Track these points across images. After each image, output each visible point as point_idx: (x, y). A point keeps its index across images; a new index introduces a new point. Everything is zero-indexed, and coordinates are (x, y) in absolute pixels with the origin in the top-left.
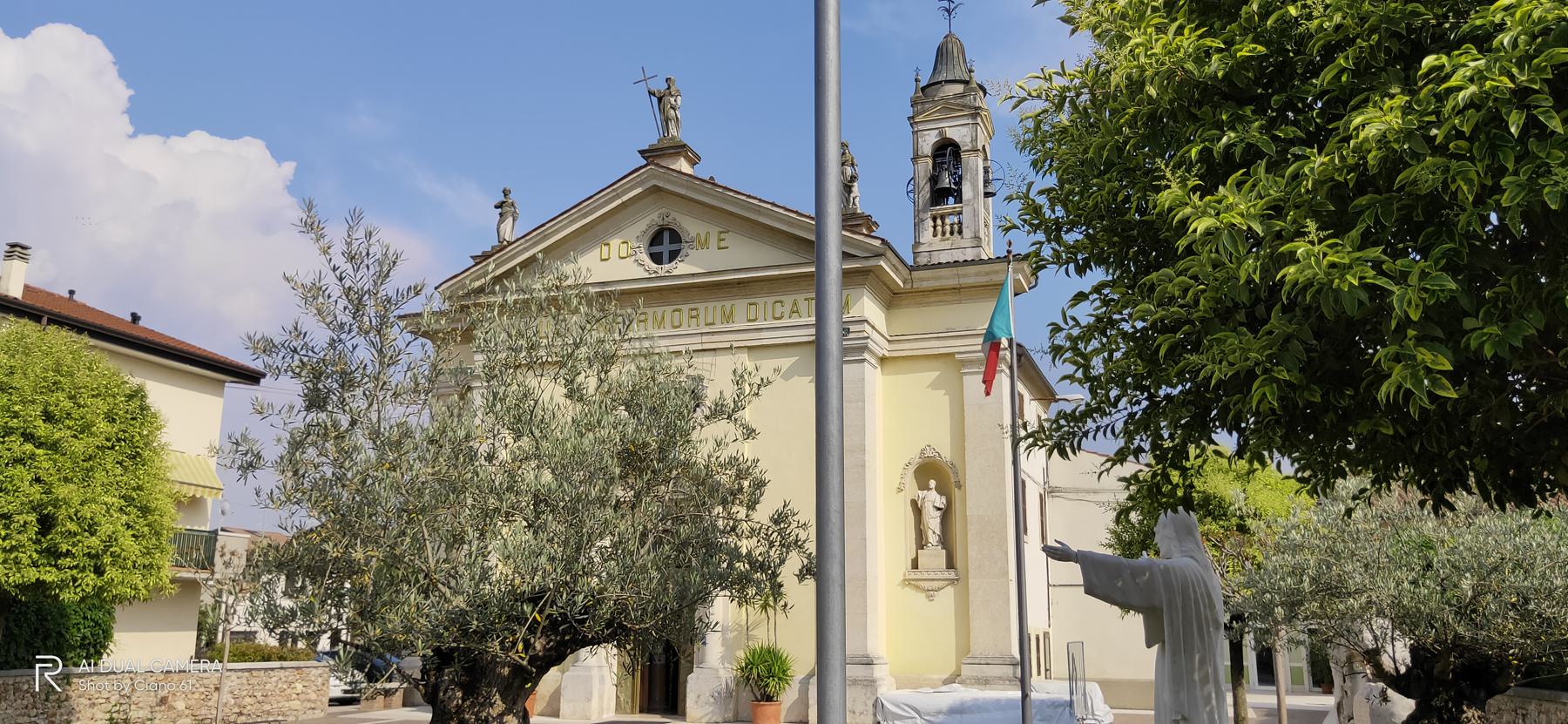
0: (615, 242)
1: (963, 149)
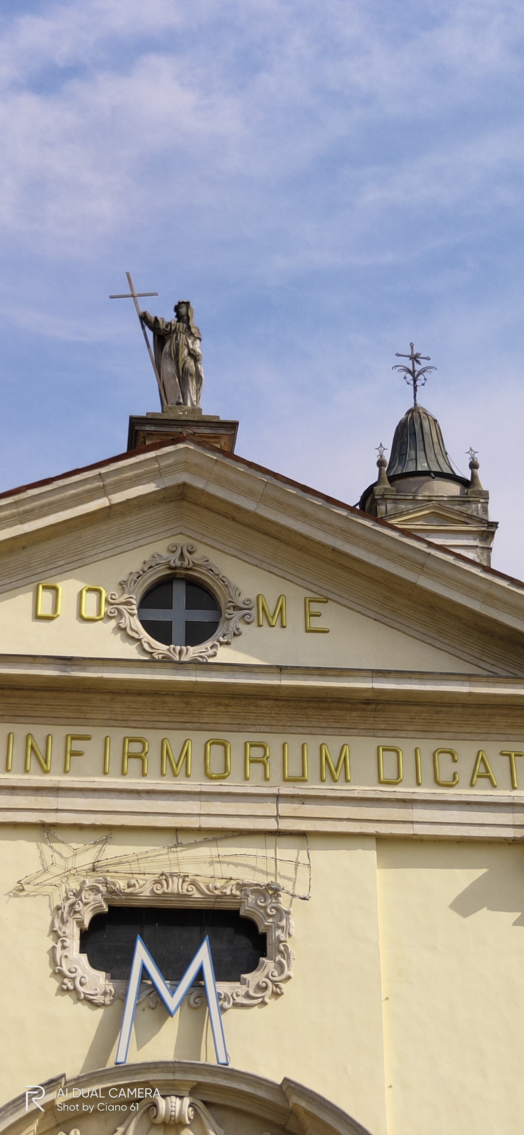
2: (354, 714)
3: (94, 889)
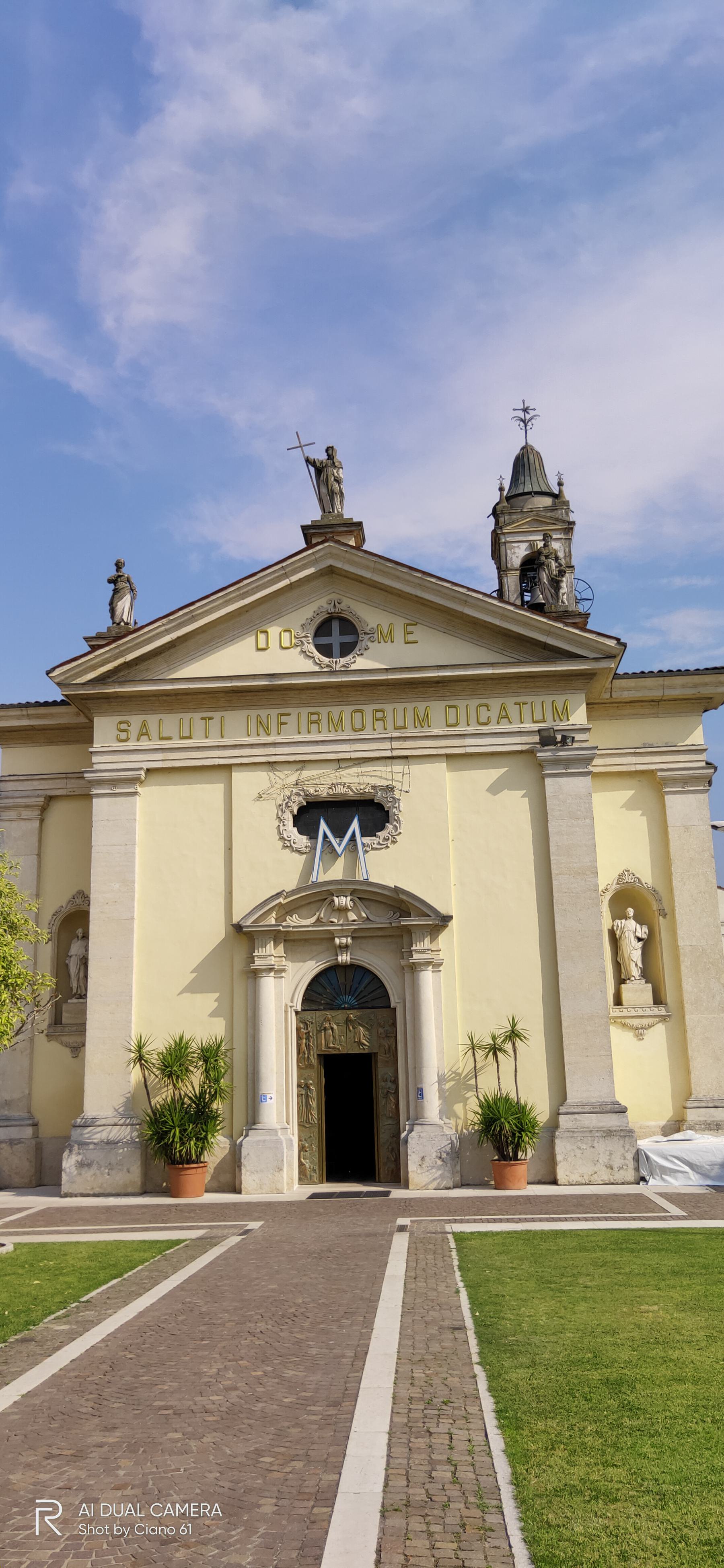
0: (274, 631)
2: (431, 689)
3: (298, 794)
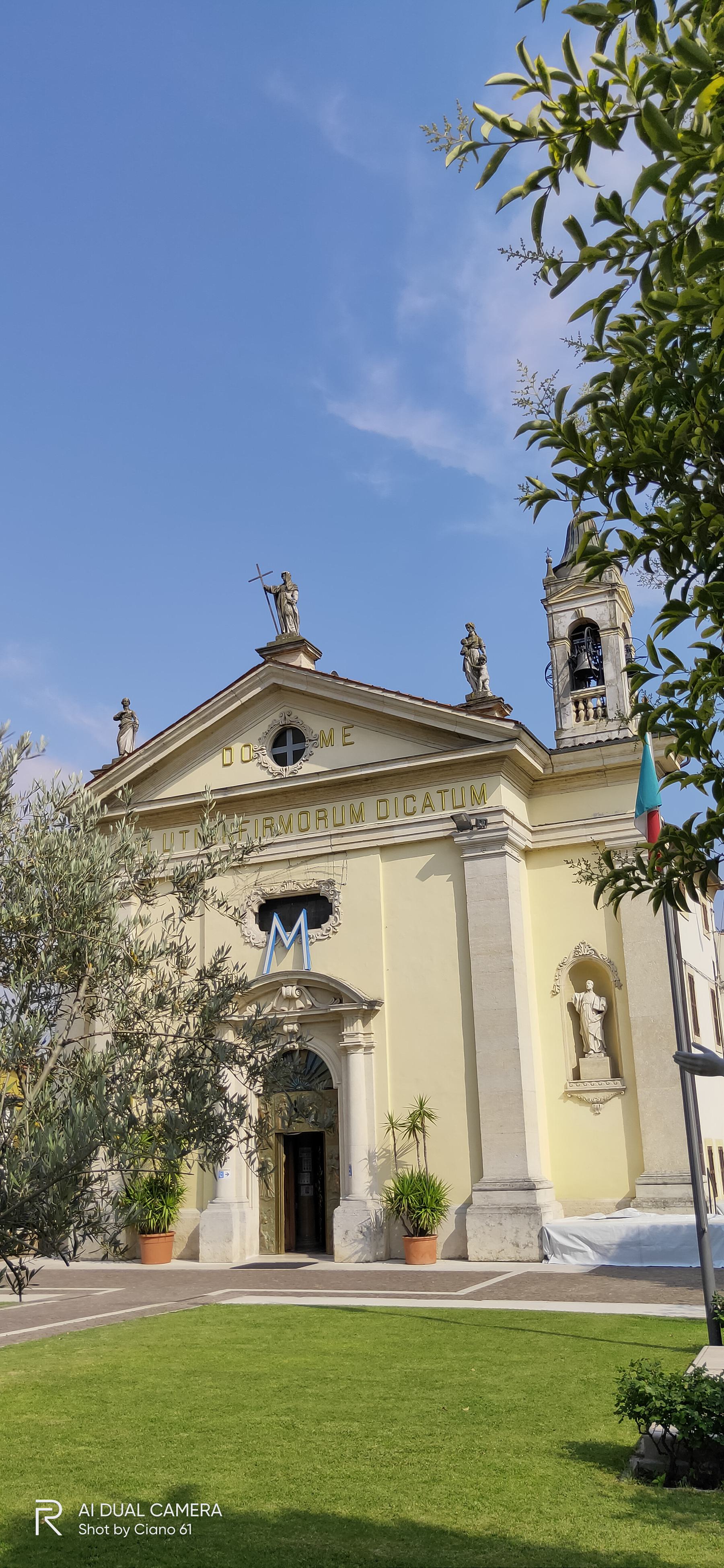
0: (237, 746)
1: (601, 628)
3: (256, 894)
